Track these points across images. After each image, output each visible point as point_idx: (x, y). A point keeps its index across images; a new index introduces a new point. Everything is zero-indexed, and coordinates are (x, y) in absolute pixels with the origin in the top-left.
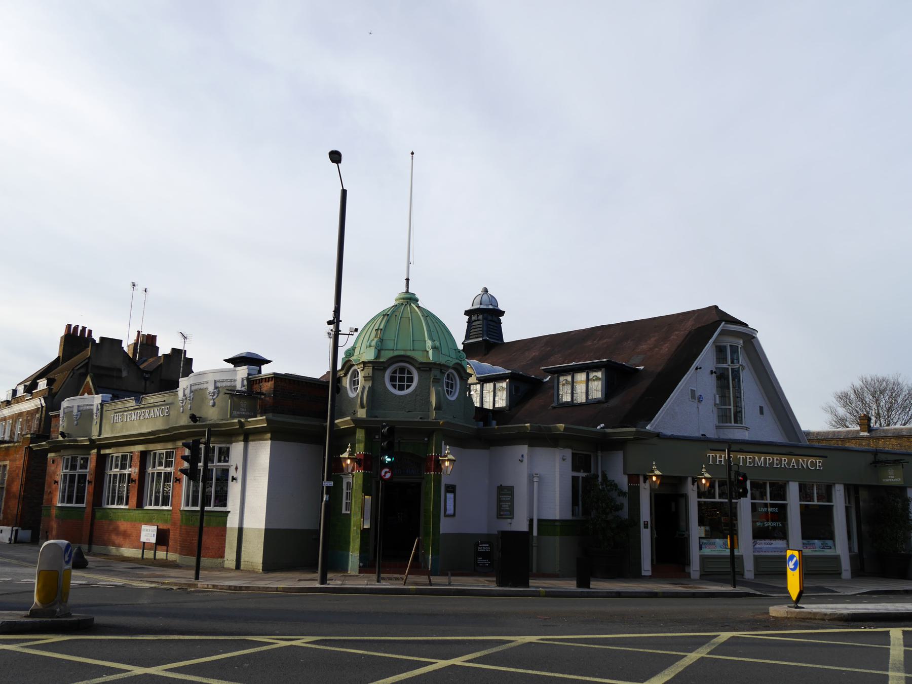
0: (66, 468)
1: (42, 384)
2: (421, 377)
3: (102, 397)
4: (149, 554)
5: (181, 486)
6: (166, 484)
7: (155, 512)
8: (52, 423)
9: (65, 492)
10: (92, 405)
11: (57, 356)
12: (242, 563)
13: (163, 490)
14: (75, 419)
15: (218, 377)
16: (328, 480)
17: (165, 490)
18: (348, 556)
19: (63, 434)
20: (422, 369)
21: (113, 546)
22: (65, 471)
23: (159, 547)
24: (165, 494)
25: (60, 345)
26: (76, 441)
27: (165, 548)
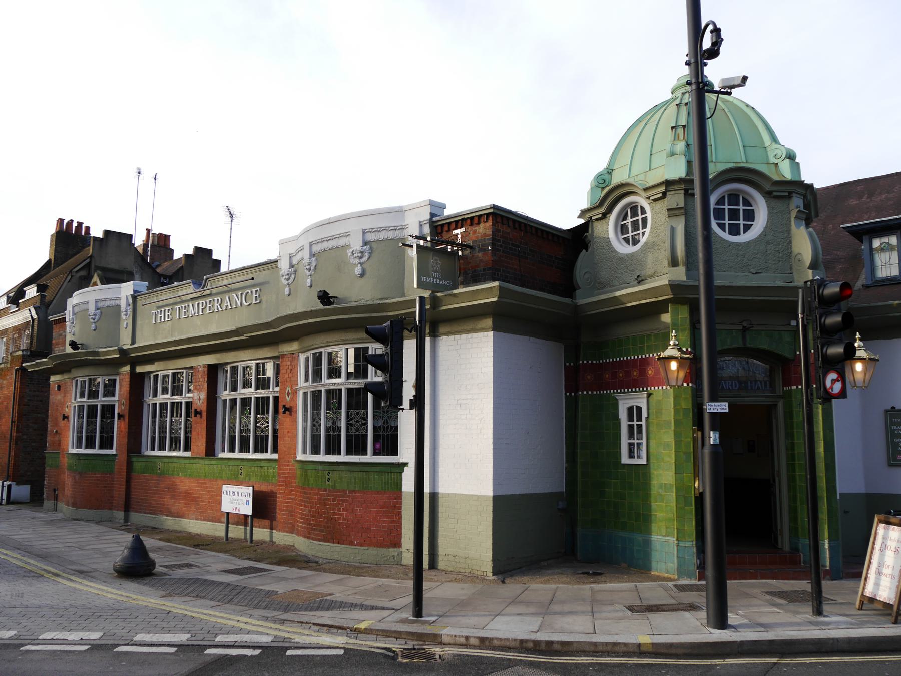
0: (82, 395)
1: (31, 292)
2: (773, 209)
3: (134, 285)
4: (237, 532)
5: (295, 420)
6: (258, 416)
7: (245, 463)
8: (54, 331)
9: (81, 432)
10: (119, 299)
11: (47, 259)
12: (440, 558)
13: (256, 427)
14: (92, 321)
15: (368, 224)
16: (713, 399)
17: (258, 427)
18: (647, 543)
19: (74, 345)
20: (775, 194)
21: (167, 516)
22: (79, 400)
23: (256, 521)
24: (259, 433)
25: (51, 245)
26: (97, 353)
27: (267, 522)
